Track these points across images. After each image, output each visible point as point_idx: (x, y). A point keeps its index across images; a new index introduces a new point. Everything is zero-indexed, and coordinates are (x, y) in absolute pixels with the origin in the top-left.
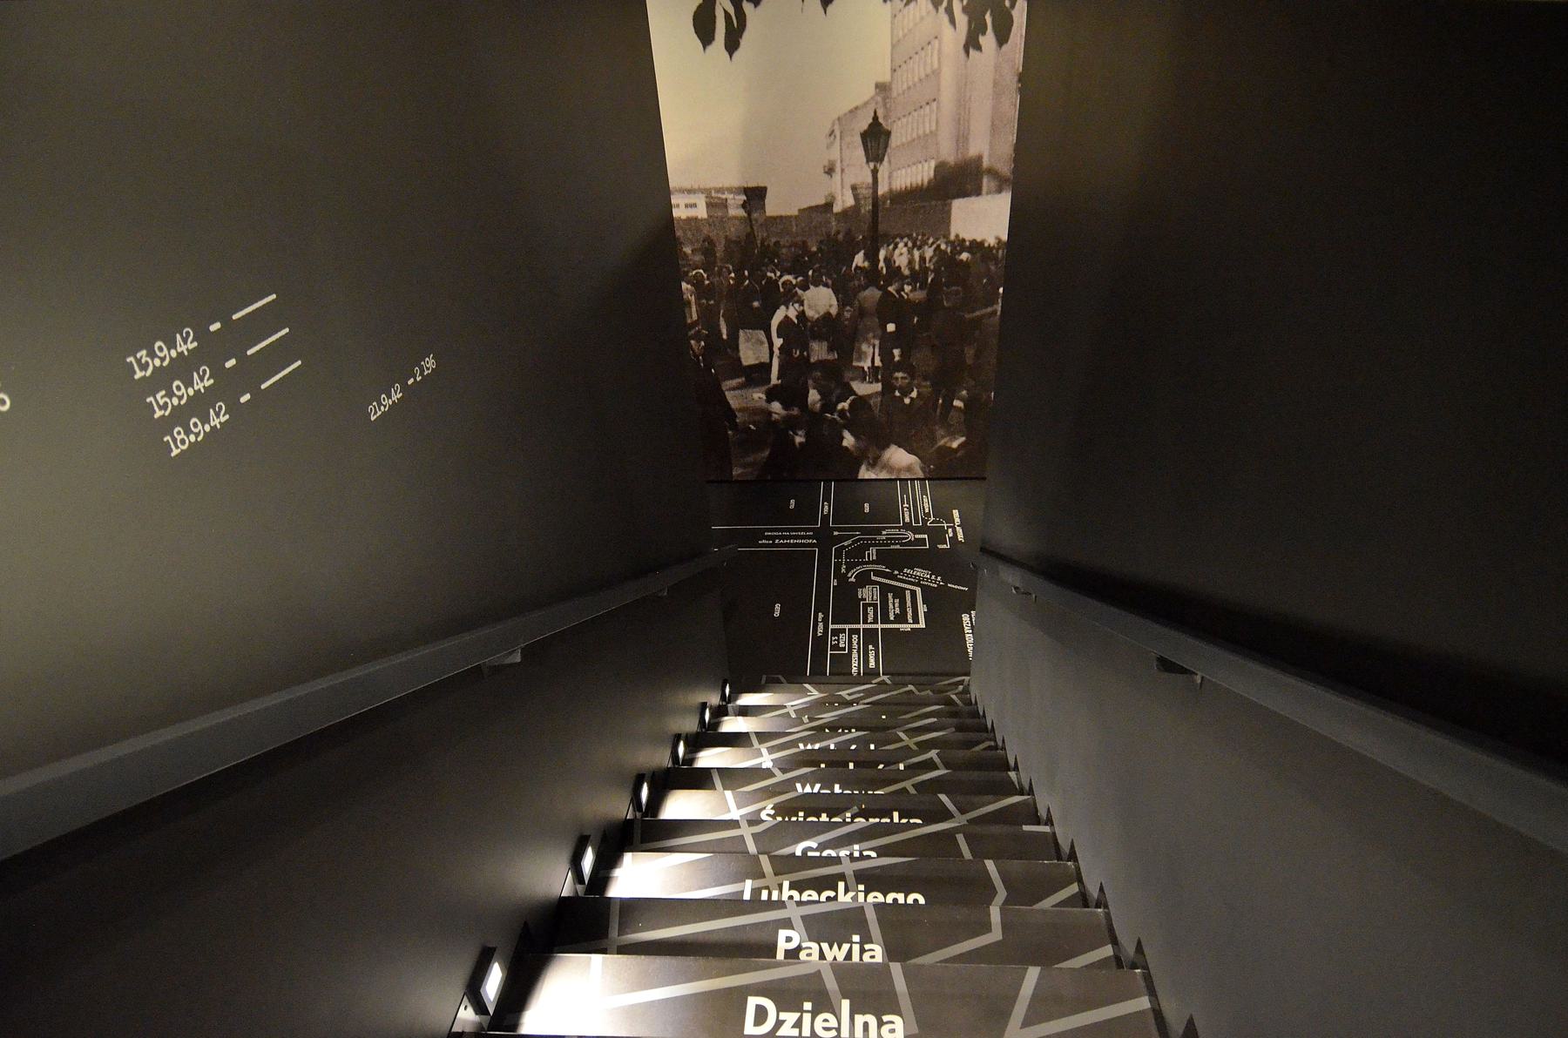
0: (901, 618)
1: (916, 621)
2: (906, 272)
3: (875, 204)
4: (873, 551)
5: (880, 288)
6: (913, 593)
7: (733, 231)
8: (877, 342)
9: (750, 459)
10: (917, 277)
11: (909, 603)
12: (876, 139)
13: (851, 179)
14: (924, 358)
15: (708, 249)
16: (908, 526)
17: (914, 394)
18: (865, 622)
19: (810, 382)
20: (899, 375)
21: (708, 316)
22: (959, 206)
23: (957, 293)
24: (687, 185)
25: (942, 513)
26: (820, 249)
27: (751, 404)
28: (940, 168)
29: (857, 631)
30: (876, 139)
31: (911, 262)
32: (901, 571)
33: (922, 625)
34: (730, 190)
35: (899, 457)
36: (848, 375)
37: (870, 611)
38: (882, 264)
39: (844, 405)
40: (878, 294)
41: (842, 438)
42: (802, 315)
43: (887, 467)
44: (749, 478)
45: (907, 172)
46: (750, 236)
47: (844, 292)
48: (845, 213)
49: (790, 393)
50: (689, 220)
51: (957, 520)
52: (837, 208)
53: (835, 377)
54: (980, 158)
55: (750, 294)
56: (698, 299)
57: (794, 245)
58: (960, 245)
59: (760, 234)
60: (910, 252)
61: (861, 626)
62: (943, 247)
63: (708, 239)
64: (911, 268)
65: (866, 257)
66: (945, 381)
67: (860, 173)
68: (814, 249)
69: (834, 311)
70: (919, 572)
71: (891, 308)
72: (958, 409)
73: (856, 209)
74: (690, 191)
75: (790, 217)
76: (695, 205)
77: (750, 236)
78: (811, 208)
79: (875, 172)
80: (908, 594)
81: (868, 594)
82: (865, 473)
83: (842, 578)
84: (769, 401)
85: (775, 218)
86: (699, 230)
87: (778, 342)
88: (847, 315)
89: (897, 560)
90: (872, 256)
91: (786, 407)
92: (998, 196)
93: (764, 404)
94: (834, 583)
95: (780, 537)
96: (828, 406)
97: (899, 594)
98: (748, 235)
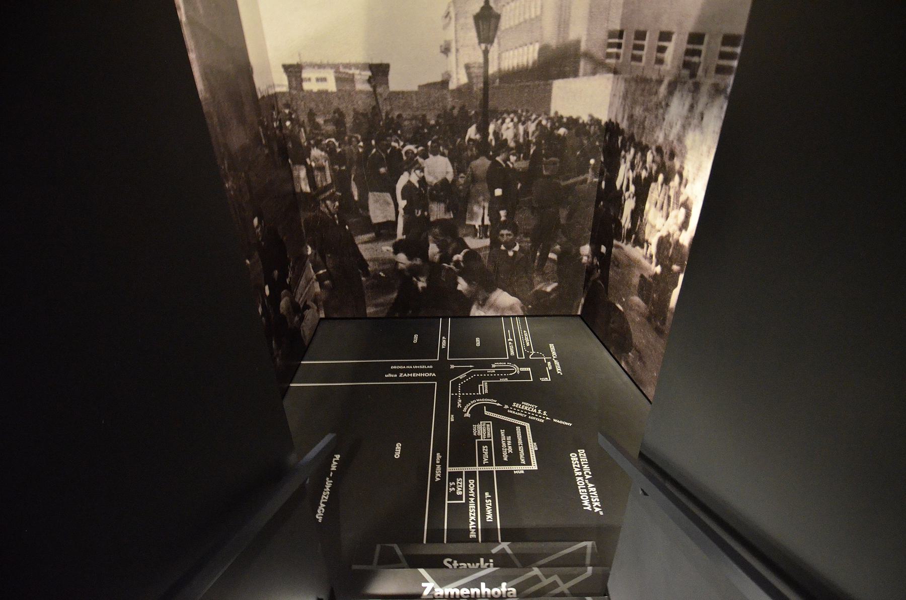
0: (514, 459)
1: (529, 463)
2: (512, 144)
3: (486, 83)
4: (485, 384)
5: (489, 158)
6: (523, 429)
7: (361, 104)
8: (486, 205)
9: (381, 300)
10: (521, 148)
11: (520, 442)
12: (487, 22)
13: (464, 59)
14: (526, 218)
15: (338, 120)
16: (513, 360)
17: (517, 248)
18: (481, 464)
19: (430, 238)
20: (505, 232)
21: (342, 181)
22: (558, 86)
23: (554, 163)
24: (317, 60)
25: (540, 346)
26: (437, 123)
27: (381, 256)
28: (543, 50)
29: (471, 475)
30: (487, 22)
31: (516, 135)
32: (510, 405)
33: (534, 466)
34: (357, 66)
35: (503, 299)
36: (461, 232)
37: (485, 448)
38: (491, 137)
39: (459, 257)
40: (488, 163)
41: (457, 284)
42: (422, 181)
43: (493, 306)
44: (381, 315)
45: (515, 54)
46: (376, 110)
47: (459, 160)
48: (459, 90)
49: (413, 246)
50: (321, 93)
51: (554, 353)
52: (452, 86)
53: (451, 233)
54: (578, 42)
55: (378, 161)
56: (332, 164)
57: (414, 118)
58: (558, 121)
59: (385, 108)
60: (516, 126)
61: (477, 469)
62: (544, 122)
63: (337, 111)
64: (517, 142)
65: (478, 130)
66: (542, 237)
67: (470, 51)
68: (433, 122)
69: (450, 177)
70: (526, 406)
71: (499, 175)
72: (552, 260)
73: (469, 86)
74: (320, 66)
75: (411, 92)
76: (324, 80)
77: (376, 110)
78: (430, 86)
79: (486, 53)
80: (518, 429)
81: (483, 430)
82: (475, 312)
83: (458, 413)
84: (396, 252)
85: (397, 94)
86: (330, 102)
87: (402, 203)
88: (461, 181)
89: (507, 393)
90: (483, 130)
91: (410, 257)
92: (592, 78)
93: (392, 256)
94: (451, 418)
95: (404, 371)
96: (446, 257)
97: (510, 429)
98: (374, 108)
